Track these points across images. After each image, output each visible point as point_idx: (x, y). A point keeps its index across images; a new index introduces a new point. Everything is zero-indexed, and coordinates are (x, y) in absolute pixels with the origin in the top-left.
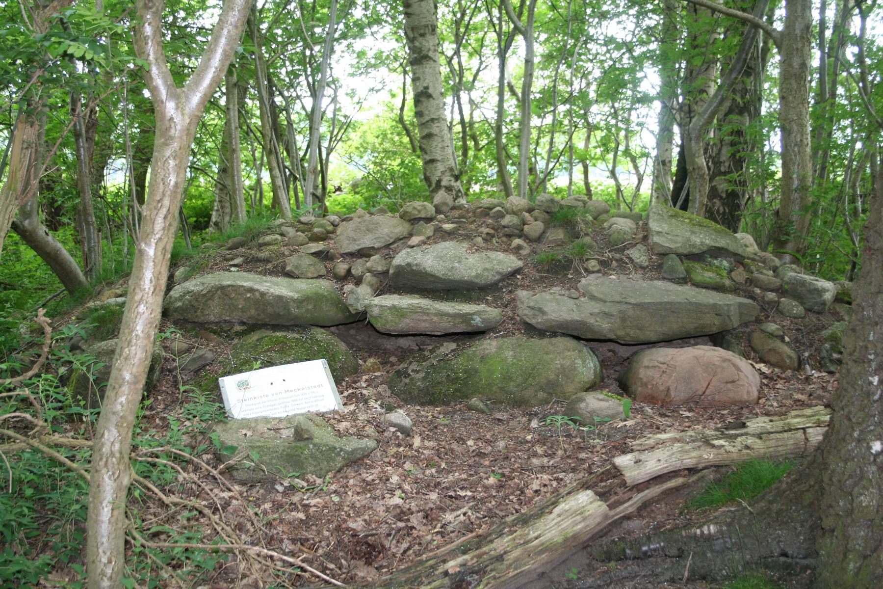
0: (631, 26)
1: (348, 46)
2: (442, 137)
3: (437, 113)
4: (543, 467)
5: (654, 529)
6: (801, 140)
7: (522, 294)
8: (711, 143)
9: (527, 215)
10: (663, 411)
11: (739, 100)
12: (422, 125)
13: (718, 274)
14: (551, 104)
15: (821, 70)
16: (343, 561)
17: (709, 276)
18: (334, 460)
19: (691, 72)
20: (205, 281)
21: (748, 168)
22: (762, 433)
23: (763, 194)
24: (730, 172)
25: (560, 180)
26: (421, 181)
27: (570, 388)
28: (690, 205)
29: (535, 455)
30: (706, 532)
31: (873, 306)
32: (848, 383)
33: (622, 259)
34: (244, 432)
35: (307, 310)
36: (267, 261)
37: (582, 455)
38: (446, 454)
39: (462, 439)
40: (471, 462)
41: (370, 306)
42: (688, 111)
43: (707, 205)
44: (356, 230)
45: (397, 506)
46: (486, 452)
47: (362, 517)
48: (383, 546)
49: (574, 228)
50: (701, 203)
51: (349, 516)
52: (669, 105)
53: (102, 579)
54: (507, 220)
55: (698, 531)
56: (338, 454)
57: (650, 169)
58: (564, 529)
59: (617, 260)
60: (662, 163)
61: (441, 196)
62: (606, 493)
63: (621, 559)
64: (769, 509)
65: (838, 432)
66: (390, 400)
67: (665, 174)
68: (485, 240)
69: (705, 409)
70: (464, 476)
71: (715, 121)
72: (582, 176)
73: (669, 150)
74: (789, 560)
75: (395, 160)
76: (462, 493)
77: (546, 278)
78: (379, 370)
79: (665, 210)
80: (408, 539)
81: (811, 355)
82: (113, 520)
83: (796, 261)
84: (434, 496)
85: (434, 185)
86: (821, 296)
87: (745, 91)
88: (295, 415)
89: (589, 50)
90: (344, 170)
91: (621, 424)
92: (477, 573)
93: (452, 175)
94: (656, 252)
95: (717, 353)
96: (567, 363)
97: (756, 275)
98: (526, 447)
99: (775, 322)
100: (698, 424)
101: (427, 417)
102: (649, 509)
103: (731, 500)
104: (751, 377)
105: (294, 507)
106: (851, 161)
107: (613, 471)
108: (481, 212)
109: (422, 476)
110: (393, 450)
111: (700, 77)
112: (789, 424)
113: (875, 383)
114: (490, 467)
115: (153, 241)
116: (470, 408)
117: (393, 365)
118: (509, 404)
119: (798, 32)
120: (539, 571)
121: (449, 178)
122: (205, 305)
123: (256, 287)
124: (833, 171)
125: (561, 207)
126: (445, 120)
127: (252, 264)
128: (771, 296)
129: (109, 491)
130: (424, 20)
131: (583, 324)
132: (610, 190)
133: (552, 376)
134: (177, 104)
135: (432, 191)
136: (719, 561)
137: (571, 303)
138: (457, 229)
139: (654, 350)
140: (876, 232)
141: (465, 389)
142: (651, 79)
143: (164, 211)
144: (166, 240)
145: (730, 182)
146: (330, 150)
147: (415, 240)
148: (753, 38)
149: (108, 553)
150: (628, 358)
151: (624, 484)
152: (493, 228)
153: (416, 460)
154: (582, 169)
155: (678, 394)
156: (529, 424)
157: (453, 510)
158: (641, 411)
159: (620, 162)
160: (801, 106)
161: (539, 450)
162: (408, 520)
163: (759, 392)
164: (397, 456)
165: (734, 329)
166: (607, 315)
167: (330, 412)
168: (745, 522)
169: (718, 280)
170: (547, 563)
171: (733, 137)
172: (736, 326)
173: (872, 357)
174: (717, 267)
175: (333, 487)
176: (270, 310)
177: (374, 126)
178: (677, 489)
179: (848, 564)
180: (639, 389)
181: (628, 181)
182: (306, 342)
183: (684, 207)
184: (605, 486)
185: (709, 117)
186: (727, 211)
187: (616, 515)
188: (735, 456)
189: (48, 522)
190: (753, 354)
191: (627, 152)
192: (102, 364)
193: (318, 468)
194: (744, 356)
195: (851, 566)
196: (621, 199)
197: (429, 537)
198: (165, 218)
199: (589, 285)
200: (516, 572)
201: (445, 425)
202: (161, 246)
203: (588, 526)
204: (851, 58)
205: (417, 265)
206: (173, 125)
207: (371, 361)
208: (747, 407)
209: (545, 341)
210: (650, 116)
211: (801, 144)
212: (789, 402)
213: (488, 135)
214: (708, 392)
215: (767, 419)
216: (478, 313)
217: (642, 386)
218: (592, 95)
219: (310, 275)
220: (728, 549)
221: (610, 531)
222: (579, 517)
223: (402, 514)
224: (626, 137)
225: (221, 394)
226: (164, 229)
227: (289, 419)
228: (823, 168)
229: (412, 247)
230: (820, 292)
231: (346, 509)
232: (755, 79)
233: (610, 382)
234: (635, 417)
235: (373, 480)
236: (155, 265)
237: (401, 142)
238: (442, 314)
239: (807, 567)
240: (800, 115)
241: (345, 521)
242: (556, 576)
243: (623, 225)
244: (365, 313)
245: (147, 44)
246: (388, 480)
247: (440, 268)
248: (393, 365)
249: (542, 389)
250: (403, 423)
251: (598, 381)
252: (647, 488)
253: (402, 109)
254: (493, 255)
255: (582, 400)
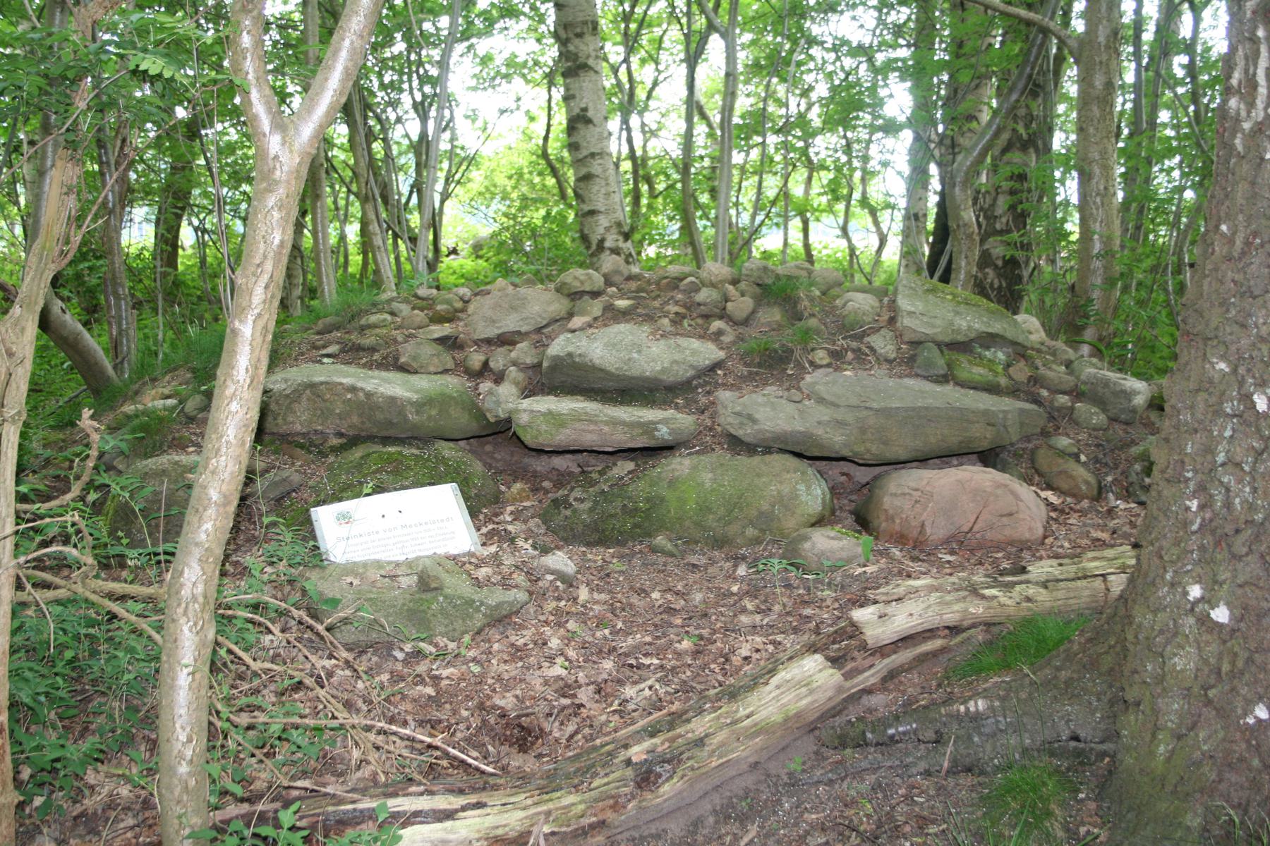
0: (871, 22)
1: (470, 48)
2: (606, 179)
3: (600, 146)
4: (755, 627)
5: (904, 705)
6: (1106, 188)
7: (724, 395)
8: (983, 190)
9: (731, 287)
10: (916, 553)
11: (1021, 130)
12: (577, 163)
13: (991, 370)
14: (758, 133)
15: (1137, 87)
16: (490, 748)
17: (979, 372)
18: (471, 618)
19: (956, 91)
20: (289, 376)
21: (1033, 225)
22: (1048, 581)
23: (1053, 262)
24: (1009, 231)
25: (770, 241)
26: (573, 240)
27: (790, 523)
28: (953, 276)
29: (744, 610)
30: (972, 709)
31: (1192, 407)
32: (1159, 509)
33: (860, 349)
34: (349, 580)
35: (430, 417)
36: (373, 350)
37: (808, 611)
38: (623, 610)
39: (644, 591)
40: (657, 620)
41: (517, 411)
42: (951, 146)
43: (976, 277)
44: (497, 306)
45: (559, 678)
46: (678, 607)
47: (513, 692)
48: (541, 730)
49: (795, 306)
50: (968, 272)
51: (494, 690)
52: (925, 136)
53: (179, 763)
54: (704, 295)
55: (962, 708)
56: (478, 610)
57: (898, 226)
58: (784, 705)
59: (853, 351)
60: (914, 217)
61: (609, 262)
62: (840, 657)
63: (859, 746)
64: (1056, 677)
65: (1146, 575)
66: (545, 539)
67: (919, 233)
68: (674, 322)
69: (972, 551)
70: (648, 639)
71: (989, 160)
72: (801, 235)
73: (923, 199)
74: (1082, 745)
75: (537, 210)
76: (646, 661)
77: (757, 373)
78: (528, 499)
79: (919, 283)
80: (578, 720)
81: (1115, 479)
82: (194, 685)
83: (1097, 352)
84: (608, 665)
85: (594, 247)
86: (1130, 401)
87: (1030, 118)
88: (418, 558)
89: (812, 58)
90: (465, 223)
91: (860, 570)
92: (669, 762)
93: (620, 233)
94: (906, 339)
95: (989, 476)
96: (786, 489)
97: (1042, 370)
98: (732, 601)
99: (1068, 435)
100: (963, 570)
101: (595, 562)
102: (896, 681)
103: (1006, 667)
104: (1034, 509)
105: (419, 679)
106: (1178, 215)
107: (849, 629)
108: (668, 284)
109: (591, 639)
110: (551, 605)
111: (969, 97)
112: (1084, 569)
113: (1194, 509)
114: (683, 627)
115: (250, 319)
116: (654, 550)
117: (547, 492)
118: (707, 544)
119: (1102, 39)
120: (752, 760)
121: (615, 237)
122: (289, 409)
123: (360, 385)
124: (1154, 231)
125: (778, 277)
126: (610, 155)
127: (352, 353)
128: (1063, 400)
129: (188, 642)
130: (581, 14)
131: (808, 436)
132: (839, 255)
133: (765, 507)
134: (283, 138)
135: (592, 255)
136: (989, 747)
137: (790, 408)
138: (635, 307)
139: (903, 471)
140: (1196, 311)
141: (646, 524)
142: (898, 99)
143: (266, 278)
144: (267, 316)
145: (1009, 244)
146: (445, 196)
147: (577, 322)
148: (1042, 45)
149: (188, 729)
150: (868, 483)
151: (864, 646)
152: (685, 306)
153: (583, 618)
154: (800, 225)
155: (937, 531)
156: (734, 571)
157: (635, 683)
158: (885, 554)
159: (854, 215)
160: (1105, 141)
161: (750, 605)
162: (574, 696)
163: (1045, 528)
164: (557, 612)
165: (1012, 444)
166: (840, 423)
167: (464, 555)
168: (1023, 695)
169: (991, 378)
170: (762, 749)
171: (1012, 183)
172: (1014, 439)
173: (1190, 475)
174: (989, 360)
175: (472, 654)
176: (380, 416)
177: (503, 162)
178: (934, 654)
179: (1158, 746)
180: (884, 525)
181: (865, 242)
182: (428, 460)
183: (945, 279)
184: (839, 649)
185: (980, 154)
186: (1005, 284)
187: (853, 687)
188: (1011, 611)
189: (88, 700)
190: (1037, 478)
191: (864, 202)
192: (150, 489)
193: (451, 628)
194: (1025, 481)
195: (1162, 749)
196: (856, 267)
197: (604, 718)
198: (266, 287)
199: (816, 383)
200: (721, 761)
201: (622, 572)
202: (261, 323)
203: (815, 701)
204: (1180, 73)
205: (580, 355)
206: (278, 165)
207: (518, 486)
208: (1029, 548)
209: (756, 460)
210: (896, 152)
211: (1107, 194)
212: (1085, 542)
213: (668, 177)
214: (976, 529)
215: (1054, 562)
216: (664, 421)
217: (887, 520)
218: (817, 123)
219: (432, 369)
220: (1001, 731)
221: (845, 708)
222: (804, 690)
223: (566, 689)
224: (863, 180)
225: (313, 530)
226: (264, 302)
227: (409, 564)
228: (1138, 228)
229: (574, 331)
230: (1128, 395)
231: (490, 681)
232: (1045, 101)
233: (844, 515)
234: (878, 562)
235: (526, 645)
236: (252, 349)
237: (544, 185)
238: (615, 423)
239: (1104, 754)
240: (1104, 154)
241: (489, 697)
242: (773, 767)
243: (860, 303)
244: (509, 421)
245: (245, 58)
246: (545, 644)
247: (612, 360)
248: (547, 492)
249: (751, 523)
250: (564, 568)
251: (827, 514)
252: (895, 652)
253: (546, 138)
254: (683, 342)
255: (806, 538)
